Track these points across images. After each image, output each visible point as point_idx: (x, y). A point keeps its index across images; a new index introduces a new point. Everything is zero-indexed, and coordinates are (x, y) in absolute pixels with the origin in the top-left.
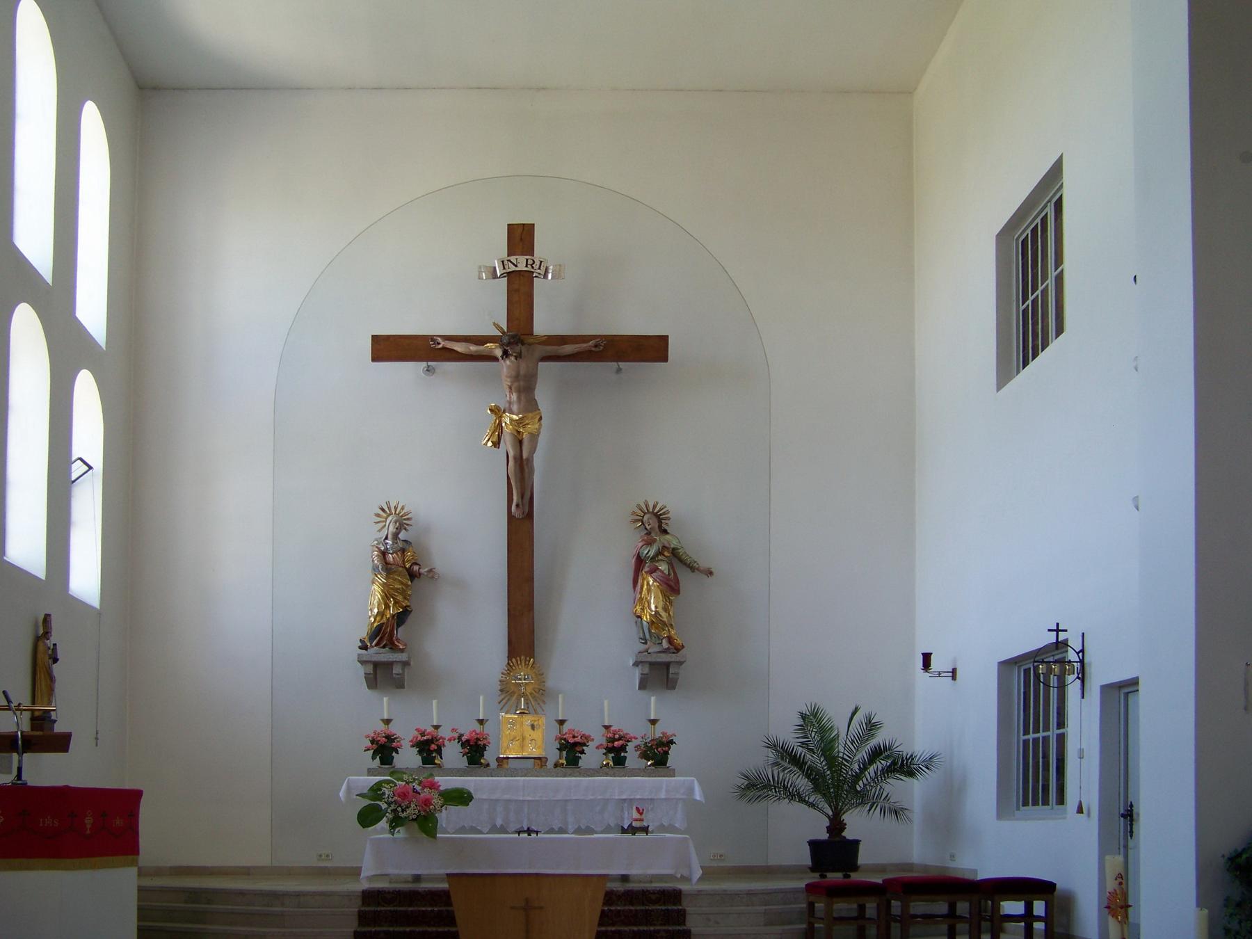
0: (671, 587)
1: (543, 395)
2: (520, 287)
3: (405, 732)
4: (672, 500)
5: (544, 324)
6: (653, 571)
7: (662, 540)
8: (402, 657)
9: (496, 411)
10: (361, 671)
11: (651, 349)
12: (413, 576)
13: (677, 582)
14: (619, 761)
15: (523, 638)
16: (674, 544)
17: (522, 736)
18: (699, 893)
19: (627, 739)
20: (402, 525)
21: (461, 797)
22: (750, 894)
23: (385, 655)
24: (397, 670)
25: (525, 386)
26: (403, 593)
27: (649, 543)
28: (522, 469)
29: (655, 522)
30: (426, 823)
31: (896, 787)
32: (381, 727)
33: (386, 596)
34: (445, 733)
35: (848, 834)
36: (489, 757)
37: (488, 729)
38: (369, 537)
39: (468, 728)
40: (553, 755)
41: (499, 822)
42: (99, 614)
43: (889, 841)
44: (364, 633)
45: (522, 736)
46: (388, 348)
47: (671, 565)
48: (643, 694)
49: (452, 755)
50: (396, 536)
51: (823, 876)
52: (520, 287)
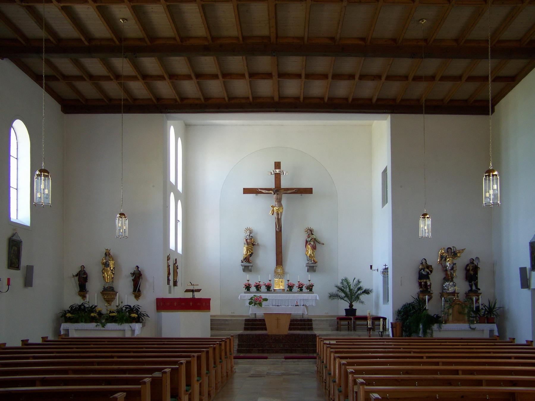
0: (314, 248)
1: (283, 202)
2: (278, 177)
3: (253, 283)
4: (313, 227)
5: (284, 184)
6: (310, 244)
7: (312, 236)
8: (251, 265)
9: (273, 207)
10: (242, 268)
11: (309, 191)
12: (253, 245)
13: (315, 246)
14: (301, 290)
15: (280, 261)
16: (315, 237)
17: (279, 285)
18: (316, 320)
19: (303, 285)
20: (250, 233)
21: (266, 300)
22: (327, 320)
23: (247, 264)
24: (250, 268)
25: (279, 201)
26: (251, 249)
27: (309, 237)
28: (279, 220)
29: (310, 232)
30: (260, 304)
31: (363, 297)
32: (247, 282)
33: (247, 250)
34: (261, 283)
35: (354, 307)
36: (272, 289)
37: (271, 282)
38: (242, 236)
39: (267, 282)
40: (287, 289)
41: (274, 304)
42: (181, 255)
43: (362, 309)
44: (242, 259)
45: (279, 285)
46: (247, 191)
47: (314, 242)
48: (308, 273)
49: (263, 288)
50: (249, 235)
51: (194, 296)
52: (278, 177)
